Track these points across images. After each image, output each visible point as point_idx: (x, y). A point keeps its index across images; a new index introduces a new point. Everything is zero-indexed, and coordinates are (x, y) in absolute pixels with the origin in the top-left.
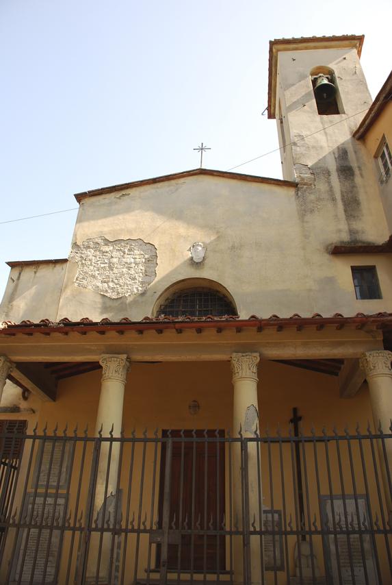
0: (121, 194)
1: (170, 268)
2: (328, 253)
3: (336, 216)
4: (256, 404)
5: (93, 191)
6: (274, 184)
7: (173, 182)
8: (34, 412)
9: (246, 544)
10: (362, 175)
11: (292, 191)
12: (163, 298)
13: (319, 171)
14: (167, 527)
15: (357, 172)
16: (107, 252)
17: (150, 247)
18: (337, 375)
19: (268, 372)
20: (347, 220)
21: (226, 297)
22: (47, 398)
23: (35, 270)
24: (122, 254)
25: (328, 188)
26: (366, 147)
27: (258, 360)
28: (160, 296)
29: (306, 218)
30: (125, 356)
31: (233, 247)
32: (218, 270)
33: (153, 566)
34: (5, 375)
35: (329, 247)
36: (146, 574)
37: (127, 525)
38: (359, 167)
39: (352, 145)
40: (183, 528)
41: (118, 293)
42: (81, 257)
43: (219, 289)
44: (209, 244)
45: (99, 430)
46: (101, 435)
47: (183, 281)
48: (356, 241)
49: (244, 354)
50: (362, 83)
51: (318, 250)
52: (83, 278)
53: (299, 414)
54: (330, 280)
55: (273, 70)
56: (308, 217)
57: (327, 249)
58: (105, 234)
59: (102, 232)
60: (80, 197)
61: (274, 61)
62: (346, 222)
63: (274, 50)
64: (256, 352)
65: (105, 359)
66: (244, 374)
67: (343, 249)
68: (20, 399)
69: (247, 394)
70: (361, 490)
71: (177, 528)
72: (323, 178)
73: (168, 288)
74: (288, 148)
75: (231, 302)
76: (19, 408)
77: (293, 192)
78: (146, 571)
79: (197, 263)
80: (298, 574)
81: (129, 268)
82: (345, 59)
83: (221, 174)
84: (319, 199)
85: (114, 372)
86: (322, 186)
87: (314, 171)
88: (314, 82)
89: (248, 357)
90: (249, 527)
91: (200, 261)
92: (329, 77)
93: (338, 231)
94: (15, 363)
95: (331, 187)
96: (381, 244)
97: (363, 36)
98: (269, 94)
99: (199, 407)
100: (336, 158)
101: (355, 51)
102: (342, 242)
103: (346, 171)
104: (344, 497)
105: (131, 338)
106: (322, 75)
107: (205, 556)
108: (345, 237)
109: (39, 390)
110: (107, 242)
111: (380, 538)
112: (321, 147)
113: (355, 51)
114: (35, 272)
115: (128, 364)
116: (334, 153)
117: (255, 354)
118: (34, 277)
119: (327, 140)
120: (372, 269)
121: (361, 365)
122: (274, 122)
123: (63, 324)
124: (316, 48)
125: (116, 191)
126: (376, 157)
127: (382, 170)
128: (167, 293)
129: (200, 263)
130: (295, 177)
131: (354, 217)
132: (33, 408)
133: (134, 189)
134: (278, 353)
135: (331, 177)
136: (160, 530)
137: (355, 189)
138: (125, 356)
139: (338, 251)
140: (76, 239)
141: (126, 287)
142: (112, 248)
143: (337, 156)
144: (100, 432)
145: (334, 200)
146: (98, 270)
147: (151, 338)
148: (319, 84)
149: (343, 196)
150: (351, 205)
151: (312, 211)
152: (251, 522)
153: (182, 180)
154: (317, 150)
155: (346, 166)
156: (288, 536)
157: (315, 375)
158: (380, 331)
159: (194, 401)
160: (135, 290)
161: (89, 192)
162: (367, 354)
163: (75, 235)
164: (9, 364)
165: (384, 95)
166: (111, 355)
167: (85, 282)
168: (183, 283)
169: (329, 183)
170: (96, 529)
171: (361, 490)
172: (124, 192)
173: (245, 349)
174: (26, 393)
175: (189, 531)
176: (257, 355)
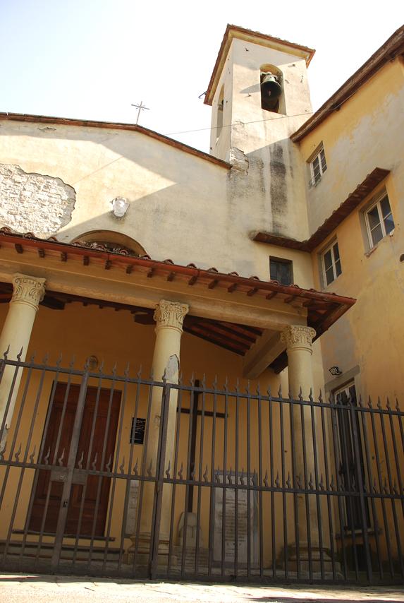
0: (45, 127)
2: (250, 238)
3: (263, 206)
4: (178, 355)
5: (14, 115)
6: (208, 160)
7: (105, 130)
9: (158, 492)
11: (224, 172)
14: (73, 466)
15: (288, 171)
17: (70, 189)
18: (243, 354)
20: (272, 212)
25: (259, 179)
26: (300, 150)
29: (235, 201)
30: (43, 280)
31: (157, 211)
35: (252, 234)
37: (25, 459)
38: (291, 167)
40: (91, 468)
41: (26, 228)
44: (133, 202)
45: (5, 351)
46: (6, 357)
50: (305, 92)
55: (224, 54)
56: (236, 200)
57: (249, 234)
59: (17, 160)
61: (226, 45)
63: (230, 35)
66: (171, 322)
67: (266, 237)
69: (170, 342)
71: (84, 467)
72: (256, 168)
74: (225, 130)
79: (118, 217)
80: (182, 544)
81: (43, 205)
82: (294, 65)
83: (157, 137)
84: (249, 186)
85: (28, 295)
86: (253, 174)
87: (249, 159)
88: (263, 77)
90: (163, 474)
91: (121, 216)
92: (276, 77)
95: (263, 179)
96: (301, 241)
97: (315, 51)
98: (213, 78)
99: (97, 362)
101: (304, 62)
105: (52, 263)
106: (270, 73)
107: (80, 520)
108: (268, 228)
110: (22, 172)
111: (395, 418)
112: (259, 139)
113: (304, 62)
116: (270, 148)
117: (183, 305)
119: (266, 134)
120: (288, 264)
121: (282, 338)
122: (209, 109)
124: (269, 46)
125: (41, 122)
126: (308, 162)
127: (313, 175)
130: (231, 158)
133: (61, 126)
134: (207, 309)
136: (65, 469)
137: (284, 186)
138: (43, 280)
139: (261, 239)
141: (35, 224)
142: (25, 180)
143: (272, 151)
145: (263, 190)
146: (6, 199)
147: (75, 267)
148: (266, 80)
150: (279, 199)
151: (241, 196)
152: (166, 469)
153: (115, 131)
155: (279, 163)
156: (202, 487)
158: (306, 309)
159: (94, 356)
160: (46, 231)
161: (10, 114)
162: (293, 327)
165: (332, 104)
166: (26, 276)
168: (99, 234)
169: (261, 174)
173: (175, 298)
175: (98, 472)
176: (187, 306)
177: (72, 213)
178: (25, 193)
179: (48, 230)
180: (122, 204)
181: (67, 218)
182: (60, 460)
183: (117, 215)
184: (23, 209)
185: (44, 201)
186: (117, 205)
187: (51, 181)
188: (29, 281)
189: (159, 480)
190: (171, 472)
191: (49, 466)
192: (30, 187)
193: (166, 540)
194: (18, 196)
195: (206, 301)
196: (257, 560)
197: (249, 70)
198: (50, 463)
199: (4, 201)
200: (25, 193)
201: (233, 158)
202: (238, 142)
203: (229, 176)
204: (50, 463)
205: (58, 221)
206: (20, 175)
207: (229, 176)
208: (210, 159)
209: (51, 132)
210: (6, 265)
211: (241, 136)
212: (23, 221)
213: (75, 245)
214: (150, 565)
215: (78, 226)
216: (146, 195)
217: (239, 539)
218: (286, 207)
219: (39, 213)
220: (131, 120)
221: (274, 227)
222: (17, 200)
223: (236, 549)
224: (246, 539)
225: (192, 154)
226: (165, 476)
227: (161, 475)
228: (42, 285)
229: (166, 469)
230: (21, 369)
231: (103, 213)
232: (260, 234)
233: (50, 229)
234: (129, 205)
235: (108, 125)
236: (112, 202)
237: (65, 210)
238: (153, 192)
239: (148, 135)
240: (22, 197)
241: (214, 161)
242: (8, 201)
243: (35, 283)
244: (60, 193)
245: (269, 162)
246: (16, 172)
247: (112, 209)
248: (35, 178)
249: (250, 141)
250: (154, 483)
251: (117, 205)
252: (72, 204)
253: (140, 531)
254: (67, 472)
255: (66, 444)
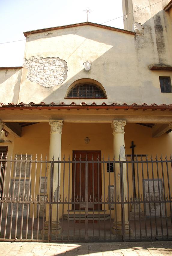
0: (48, 34)
1: (74, 72)
2: (149, 69)
3: (153, 51)
5: (33, 31)
7: (74, 28)
8: (11, 142)
10: (166, 31)
11: (132, 37)
12: (71, 88)
13: (146, 27)
15: (164, 29)
16: (42, 64)
19: (129, 129)
20: (158, 53)
21: (100, 88)
22: (18, 136)
23: (6, 72)
24: (50, 65)
26: (169, 15)
27: (126, 124)
28: (69, 87)
29: (140, 51)
31: (104, 64)
32: (97, 75)
33: (71, 209)
34: (1, 128)
35: (150, 66)
36: (68, 212)
38: (165, 26)
39: (163, 14)
40: (95, 201)
42: (29, 66)
43: (97, 84)
44: (93, 62)
45: (53, 157)
46: (54, 160)
47: (80, 79)
48: (162, 64)
49: (119, 121)
51: (145, 67)
52: (31, 77)
53: (135, 144)
54: (150, 83)
56: (140, 51)
57: (148, 67)
58: (40, 54)
60: (26, 34)
62: (158, 54)
64: (124, 120)
65: (52, 122)
67: (157, 68)
68: (4, 136)
69: (120, 140)
70: (161, 177)
71: (92, 201)
73: (73, 83)
75: (103, 91)
76: (4, 140)
77: (134, 37)
78: (68, 211)
79: (87, 71)
81: (54, 72)
84: (145, 42)
86: (147, 35)
89: (121, 122)
91: (88, 70)
93: (153, 59)
94: (5, 123)
95: (152, 36)
99: (89, 140)
100: (154, 21)
102: (156, 64)
103: (159, 28)
104: (153, 180)
105: (63, 112)
108: (157, 62)
109: (15, 133)
112: (148, 14)
114: (6, 73)
115: (63, 124)
116: (154, 18)
117: (124, 121)
118: (6, 75)
119: (151, 10)
123: (32, 105)
125: (45, 31)
128: (73, 85)
129: (88, 71)
130: (135, 28)
131: (162, 52)
132: (10, 140)
133: (54, 31)
134: (134, 121)
135: (151, 31)
136: (84, 203)
138: (61, 121)
139: (154, 69)
140: (26, 56)
141: (52, 82)
142: (44, 62)
143: (155, 20)
144: (53, 159)
145: (153, 43)
149: (157, 41)
151: (142, 48)
152: (125, 198)
153: (78, 28)
154: (146, 16)
157: (147, 129)
159: (87, 137)
160: (57, 84)
163: (25, 54)
164: (2, 124)
166: (55, 120)
167: (32, 79)
169: (151, 34)
170: (55, 203)
171: (161, 177)
172: (49, 32)
174: (7, 133)
175: (98, 202)
176: (125, 121)
177: (67, 73)
178: (45, 68)
179: (59, 83)
180: (88, 64)
181: (66, 76)
182: (82, 199)
183: (87, 70)
184: (46, 76)
185: (54, 70)
186: (86, 65)
187: (55, 59)
188: (56, 122)
189: (122, 203)
190: (127, 199)
191: (78, 202)
192: (47, 65)
193: (128, 223)
194: (43, 70)
195: (133, 117)
196: (164, 214)
197: (149, 19)
198: (79, 201)
199: (38, 74)
200: (45, 68)
201: (136, 28)
202: (137, 19)
203: (135, 39)
204: (79, 201)
205: (62, 78)
206: (42, 60)
207: (135, 39)
208: (125, 32)
209: (50, 35)
210: (45, 116)
211: (139, 14)
212: (47, 81)
213: (72, 104)
214: (123, 236)
215: (71, 79)
216: (98, 57)
217: (156, 206)
218: (164, 49)
219: (53, 76)
220: (84, 21)
221: (160, 61)
222: (43, 72)
223: (155, 211)
224: (159, 206)
225: (116, 31)
226: (125, 201)
227: (123, 201)
228: (62, 123)
229: (125, 198)
230: (60, 163)
231: (80, 71)
232: (153, 67)
233: (59, 83)
234: (91, 64)
235: (75, 25)
236: (83, 64)
237: (64, 72)
238: (101, 55)
239: (94, 26)
240: (45, 70)
241: (127, 32)
242: (39, 74)
243: (59, 122)
244: (60, 65)
245: (154, 26)
246: (40, 59)
247: (84, 68)
248: (48, 60)
249: (143, 16)
250: (120, 204)
251: (86, 65)
252: (66, 69)
253: (117, 221)
254: (86, 204)
255: (83, 193)
